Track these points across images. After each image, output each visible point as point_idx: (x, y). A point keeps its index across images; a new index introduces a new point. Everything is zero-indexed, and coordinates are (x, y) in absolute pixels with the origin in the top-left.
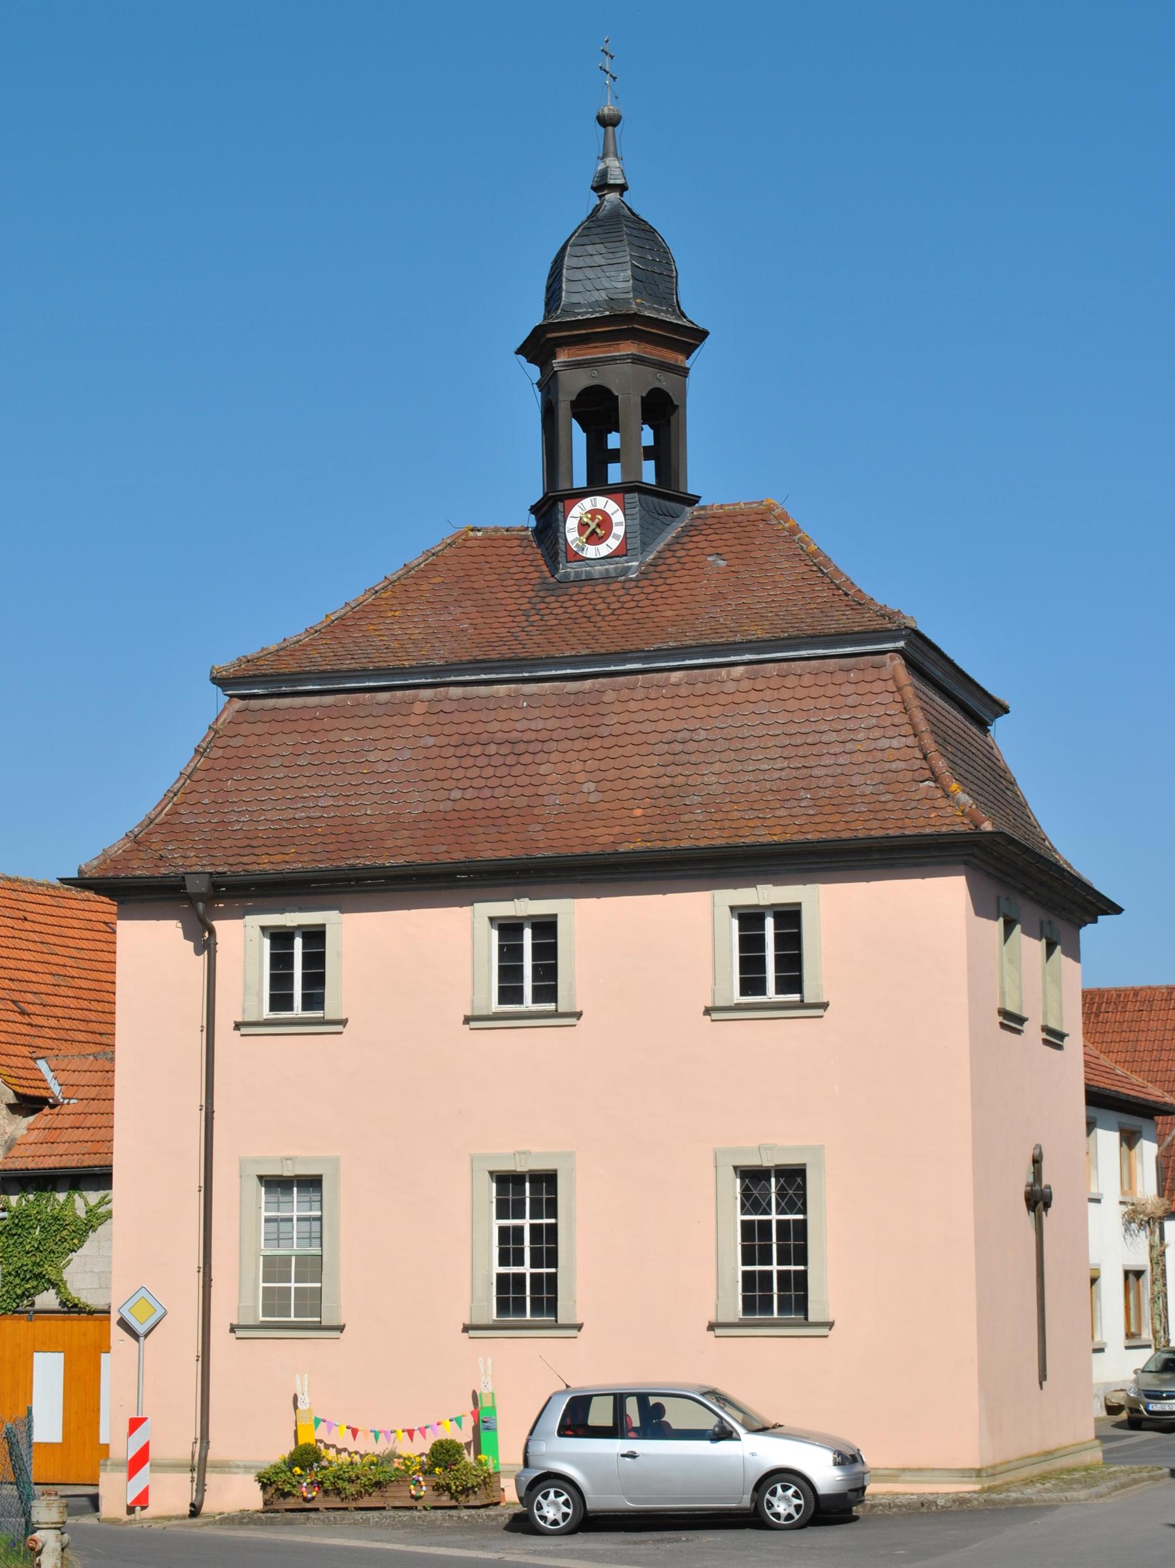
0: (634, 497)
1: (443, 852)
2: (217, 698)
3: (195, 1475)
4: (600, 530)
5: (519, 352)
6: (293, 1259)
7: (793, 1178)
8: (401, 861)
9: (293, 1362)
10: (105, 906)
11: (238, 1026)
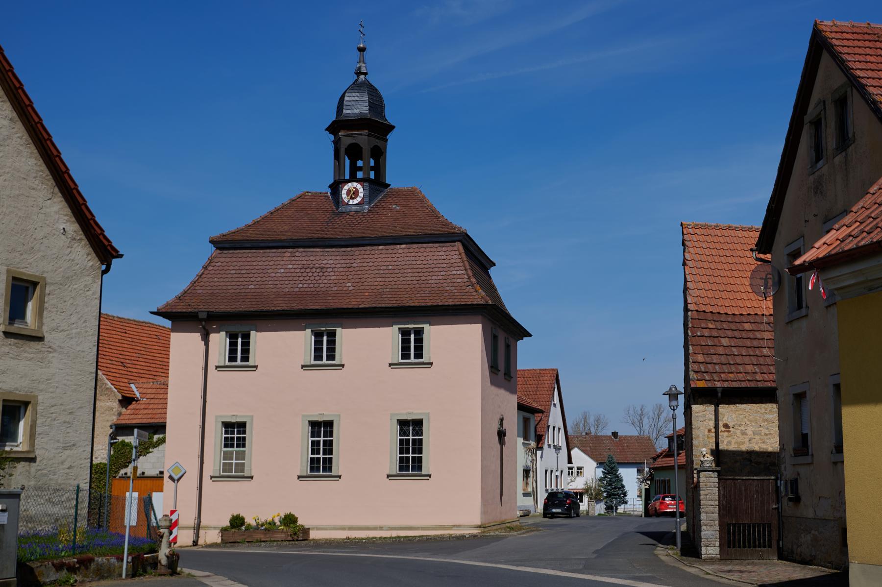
0: (366, 184)
1: (295, 306)
2: (211, 249)
4: (354, 194)
5: (327, 129)
7: (418, 424)
8: (279, 308)
10: (168, 323)
11: (217, 367)
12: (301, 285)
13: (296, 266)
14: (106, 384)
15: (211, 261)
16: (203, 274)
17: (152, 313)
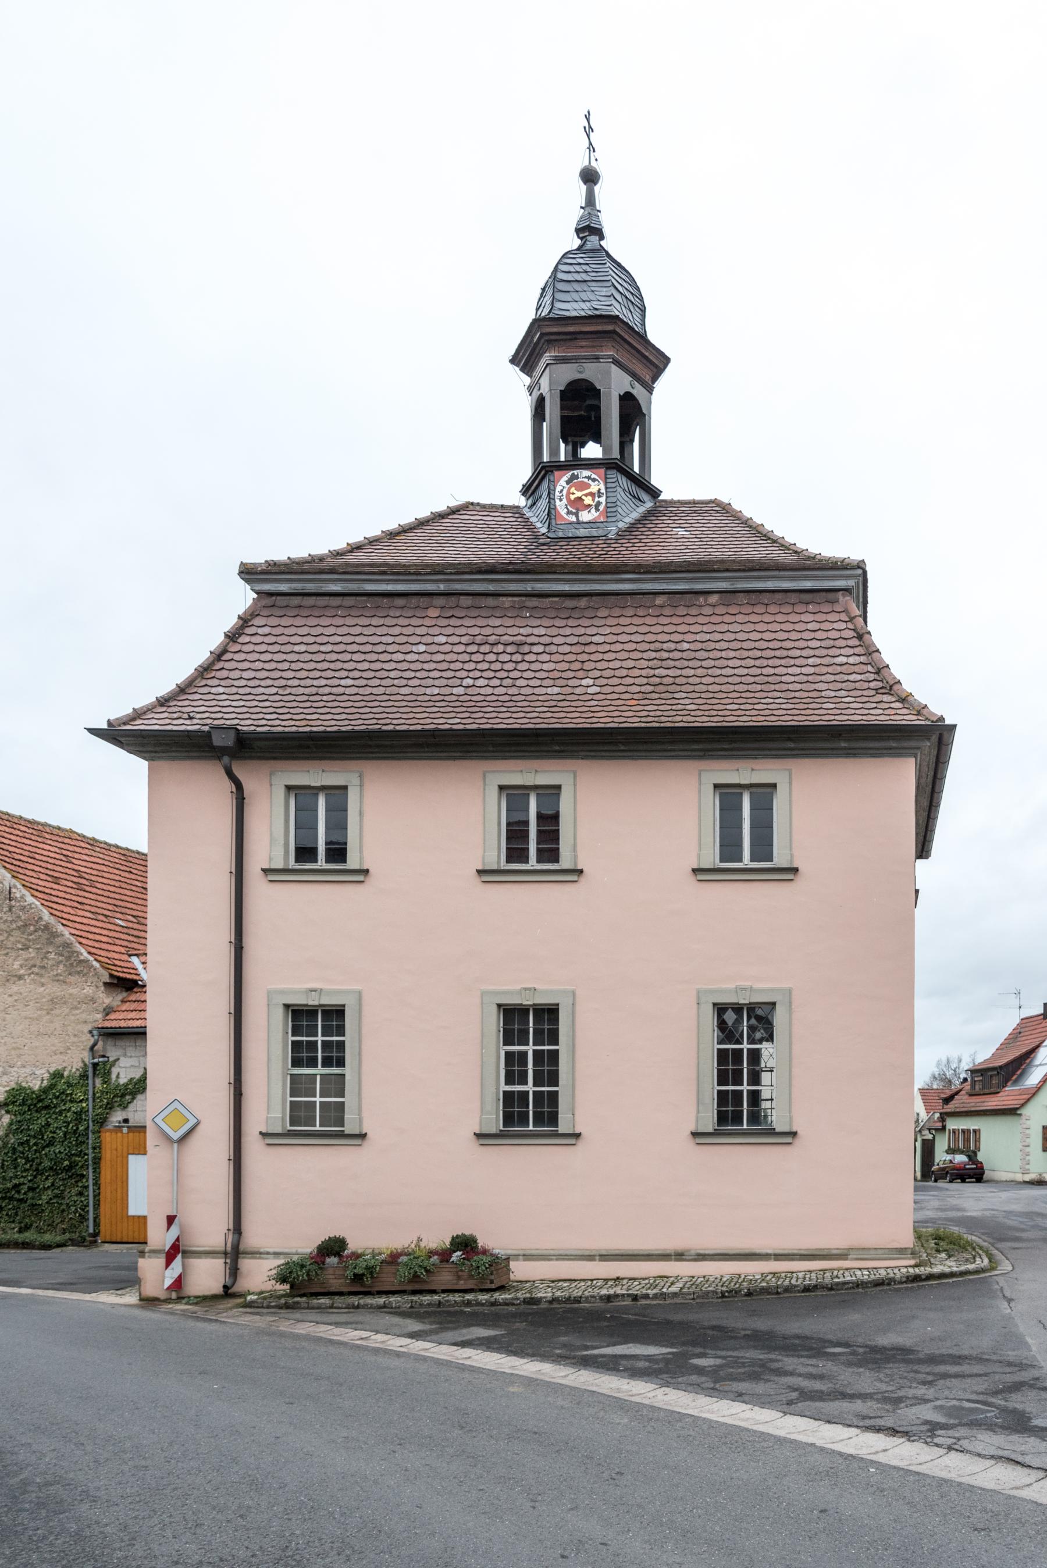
2: (244, 597)
3: (228, 1261)
6: (318, 1077)
9: (313, 1164)
11: (266, 871)
12: (469, 682)
13: (454, 639)
14: (79, 953)
15: (245, 621)
16: (225, 651)
17: (92, 731)
